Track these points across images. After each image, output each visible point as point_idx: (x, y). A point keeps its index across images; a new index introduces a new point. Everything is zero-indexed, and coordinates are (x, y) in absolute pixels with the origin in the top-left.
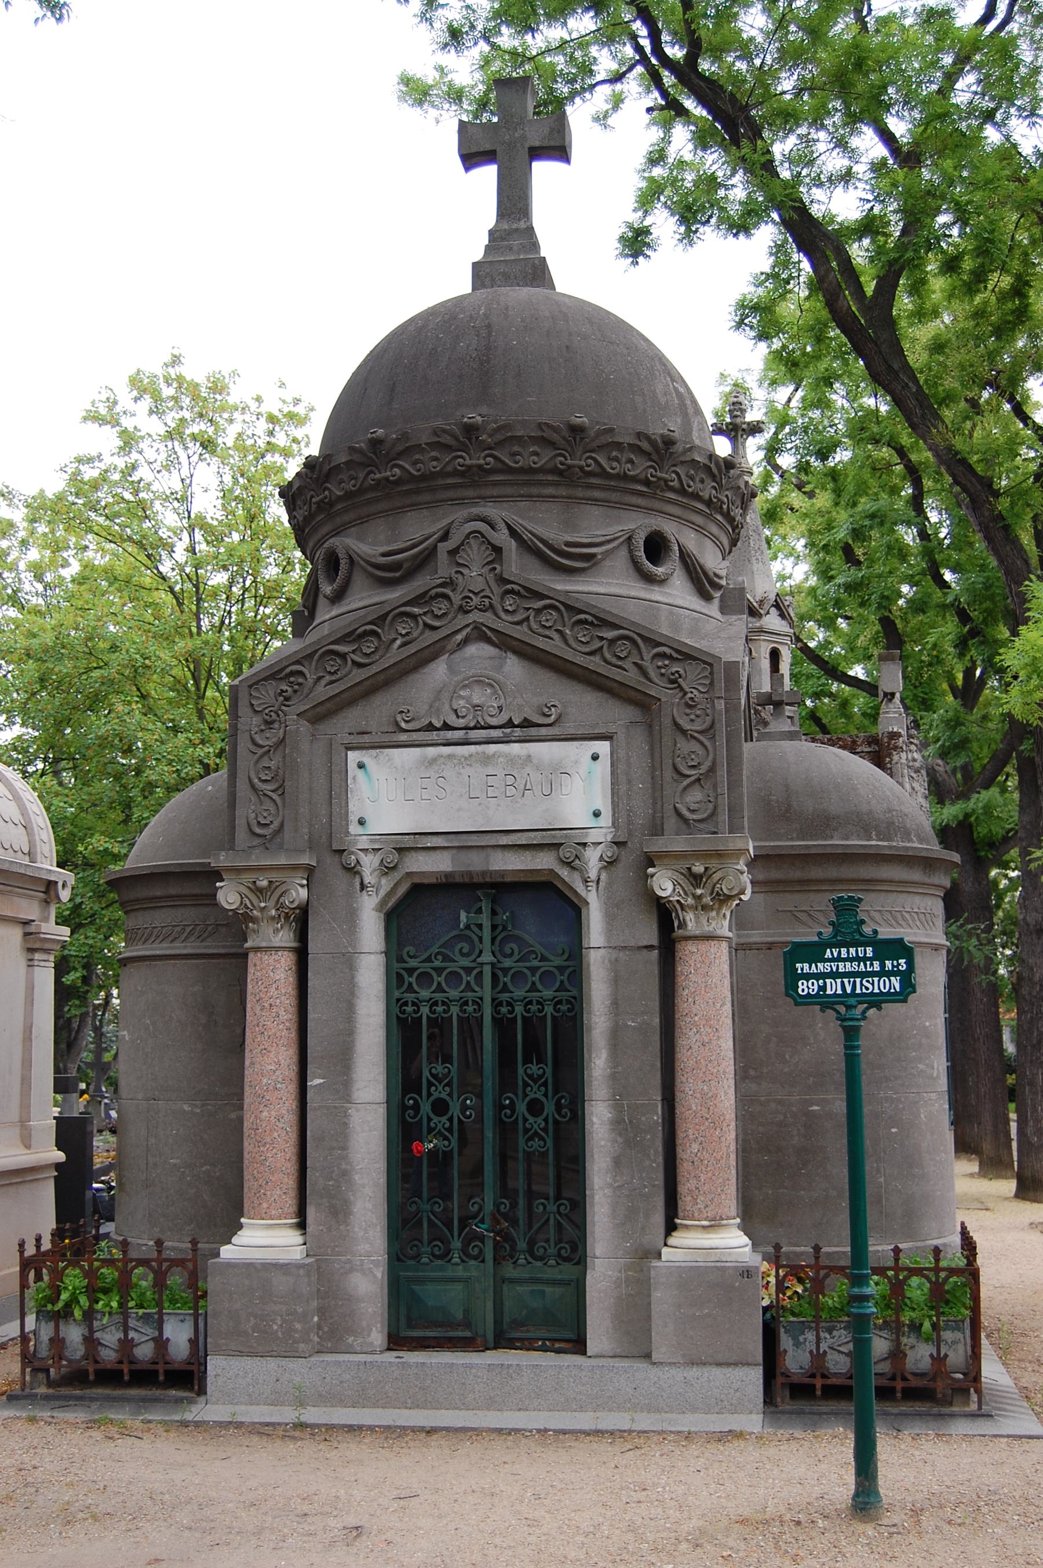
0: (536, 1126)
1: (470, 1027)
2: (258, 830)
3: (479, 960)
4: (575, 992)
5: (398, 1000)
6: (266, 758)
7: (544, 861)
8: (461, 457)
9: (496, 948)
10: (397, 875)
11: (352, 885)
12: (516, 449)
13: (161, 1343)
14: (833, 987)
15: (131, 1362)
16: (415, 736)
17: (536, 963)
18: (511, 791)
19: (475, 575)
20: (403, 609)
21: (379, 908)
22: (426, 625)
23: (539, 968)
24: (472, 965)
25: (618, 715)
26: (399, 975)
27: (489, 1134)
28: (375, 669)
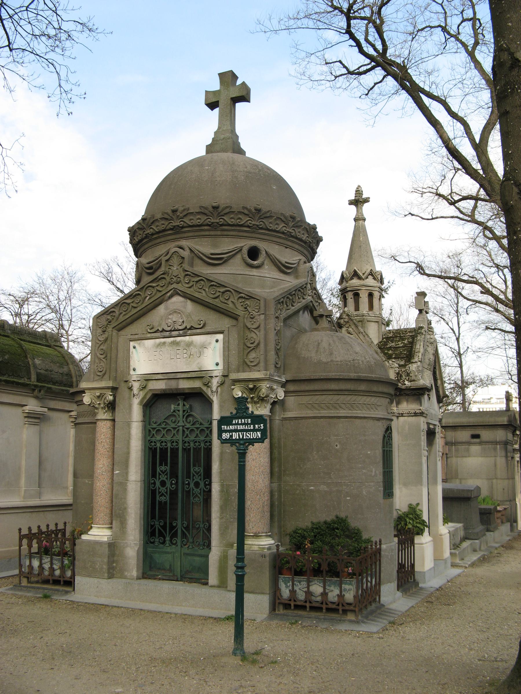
1: (174, 451)
5: (149, 440)
7: (197, 384)
8: (171, 223)
9: (184, 419)
10: (146, 391)
11: (130, 395)
12: (191, 217)
14: (235, 436)
16: (153, 335)
19: (175, 269)
20: (149, 285)
21: (141, 402)
22: (158, 290)
23: (199, 428)
24: (176, 427)
25: (226, 323)
26: (150, 430)
27: (180, 495)
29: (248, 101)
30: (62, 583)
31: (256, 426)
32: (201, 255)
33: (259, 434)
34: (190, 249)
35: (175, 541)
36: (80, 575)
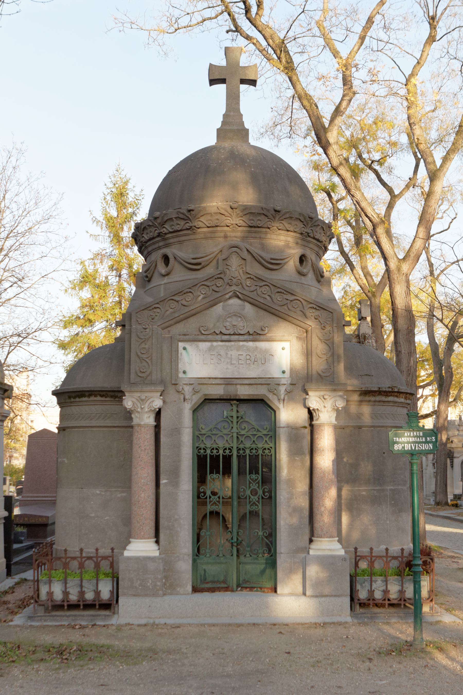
0: (254, 500)
2: (140, 375)
3: (232, 431)
4: (272, 445)
5: (197, 447)
6: (143, 344)
7: (259, 392)
13: (97, 593)
15: (68, 601)
17: (255, 433)
18: (248, 362)
28: (192, 308)
29: (255, 85)
30: (97, 607)
31: (428, 439)
32: (261, 259)
33: (431, 446)
34: (248, 250)
35: (204, 551)
36: (124, 595)
